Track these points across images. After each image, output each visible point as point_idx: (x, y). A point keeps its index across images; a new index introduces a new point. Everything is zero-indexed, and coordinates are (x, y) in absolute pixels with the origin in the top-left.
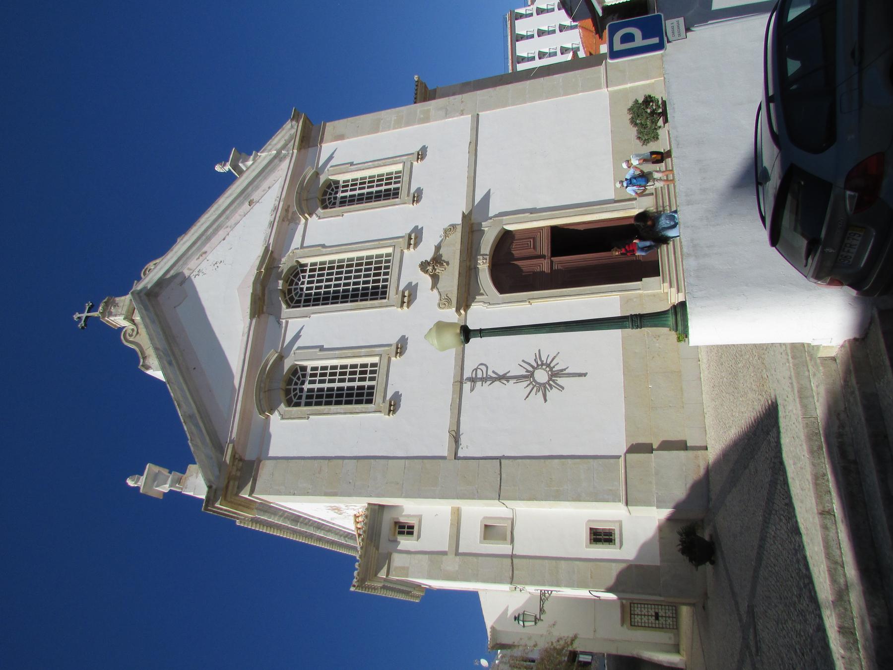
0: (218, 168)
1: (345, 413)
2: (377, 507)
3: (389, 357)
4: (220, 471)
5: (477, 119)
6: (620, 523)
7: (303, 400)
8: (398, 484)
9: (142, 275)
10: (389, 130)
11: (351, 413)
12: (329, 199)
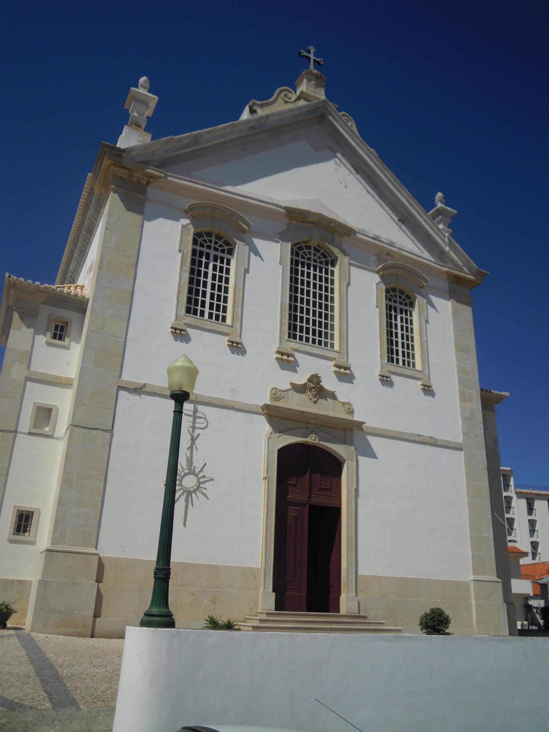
0: (439, 195)
1: (179, 286)
2: (84, 307)
3: (230, 334)
4: (140, 162)
5: (457, 448)
6: (33, 543)
7: (199, 248)
8: (102, 329)
9: (343, 113)
10: (457, 361)
11: (179, 292)
12: (396, 296)
